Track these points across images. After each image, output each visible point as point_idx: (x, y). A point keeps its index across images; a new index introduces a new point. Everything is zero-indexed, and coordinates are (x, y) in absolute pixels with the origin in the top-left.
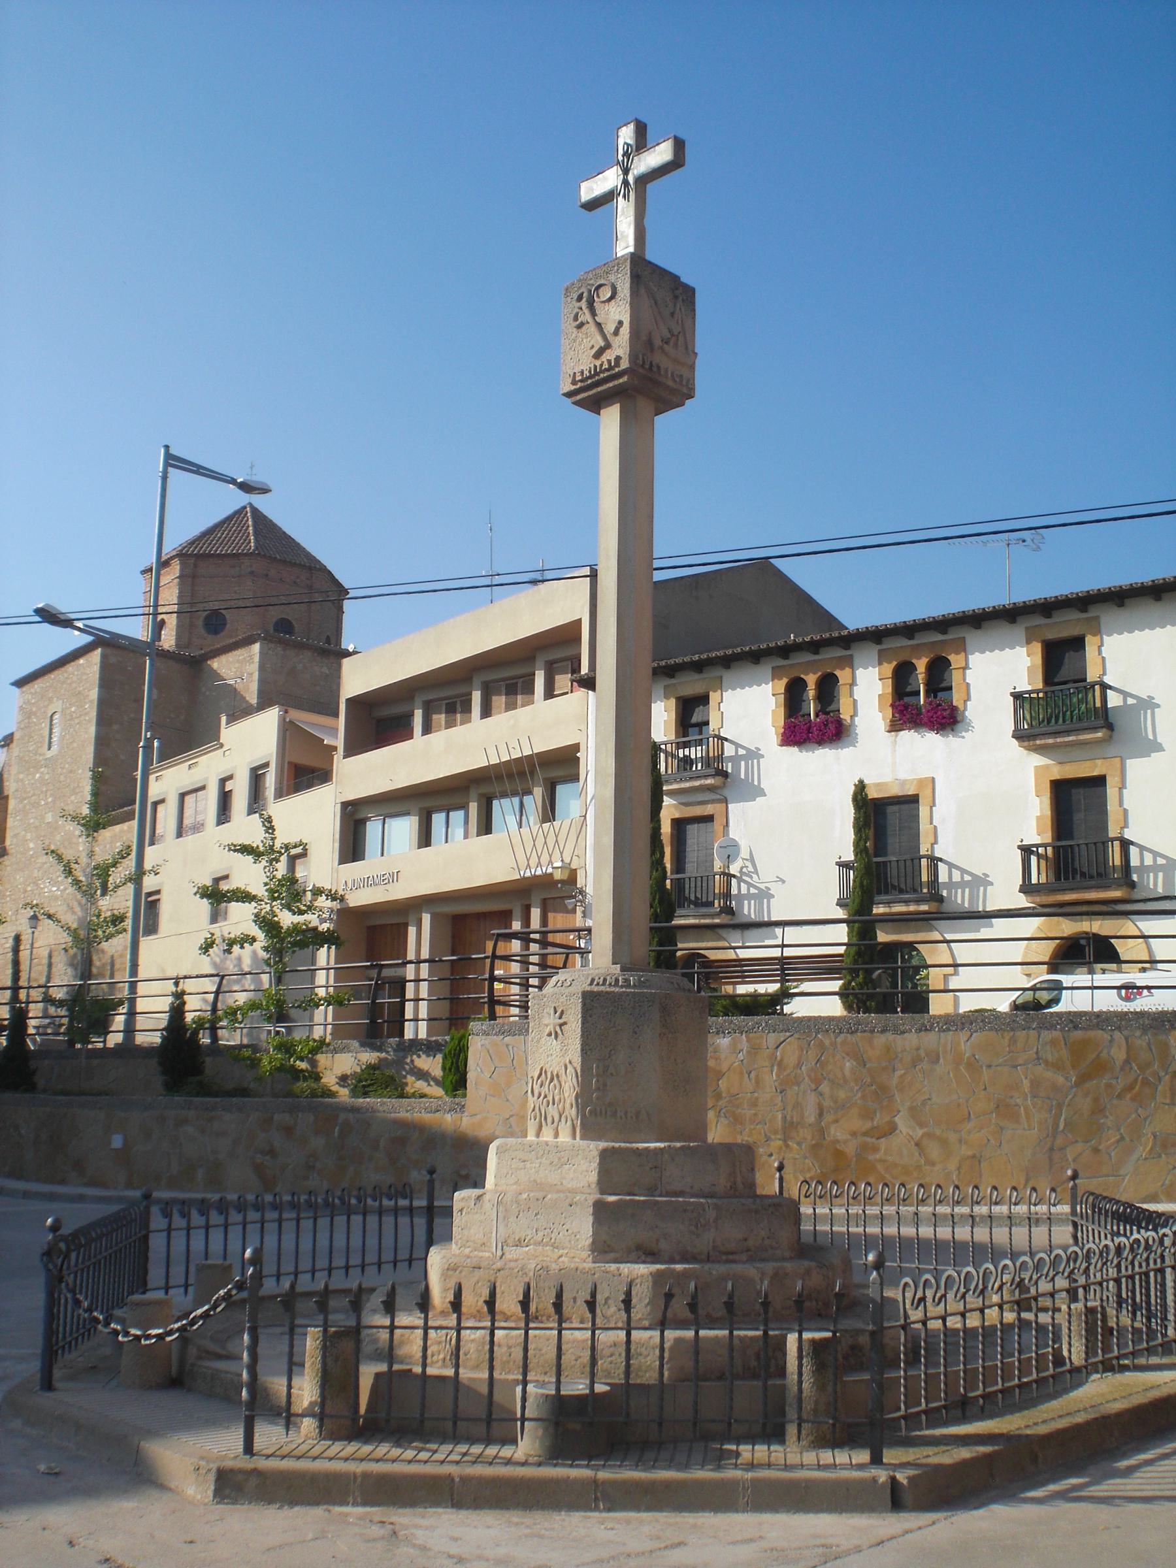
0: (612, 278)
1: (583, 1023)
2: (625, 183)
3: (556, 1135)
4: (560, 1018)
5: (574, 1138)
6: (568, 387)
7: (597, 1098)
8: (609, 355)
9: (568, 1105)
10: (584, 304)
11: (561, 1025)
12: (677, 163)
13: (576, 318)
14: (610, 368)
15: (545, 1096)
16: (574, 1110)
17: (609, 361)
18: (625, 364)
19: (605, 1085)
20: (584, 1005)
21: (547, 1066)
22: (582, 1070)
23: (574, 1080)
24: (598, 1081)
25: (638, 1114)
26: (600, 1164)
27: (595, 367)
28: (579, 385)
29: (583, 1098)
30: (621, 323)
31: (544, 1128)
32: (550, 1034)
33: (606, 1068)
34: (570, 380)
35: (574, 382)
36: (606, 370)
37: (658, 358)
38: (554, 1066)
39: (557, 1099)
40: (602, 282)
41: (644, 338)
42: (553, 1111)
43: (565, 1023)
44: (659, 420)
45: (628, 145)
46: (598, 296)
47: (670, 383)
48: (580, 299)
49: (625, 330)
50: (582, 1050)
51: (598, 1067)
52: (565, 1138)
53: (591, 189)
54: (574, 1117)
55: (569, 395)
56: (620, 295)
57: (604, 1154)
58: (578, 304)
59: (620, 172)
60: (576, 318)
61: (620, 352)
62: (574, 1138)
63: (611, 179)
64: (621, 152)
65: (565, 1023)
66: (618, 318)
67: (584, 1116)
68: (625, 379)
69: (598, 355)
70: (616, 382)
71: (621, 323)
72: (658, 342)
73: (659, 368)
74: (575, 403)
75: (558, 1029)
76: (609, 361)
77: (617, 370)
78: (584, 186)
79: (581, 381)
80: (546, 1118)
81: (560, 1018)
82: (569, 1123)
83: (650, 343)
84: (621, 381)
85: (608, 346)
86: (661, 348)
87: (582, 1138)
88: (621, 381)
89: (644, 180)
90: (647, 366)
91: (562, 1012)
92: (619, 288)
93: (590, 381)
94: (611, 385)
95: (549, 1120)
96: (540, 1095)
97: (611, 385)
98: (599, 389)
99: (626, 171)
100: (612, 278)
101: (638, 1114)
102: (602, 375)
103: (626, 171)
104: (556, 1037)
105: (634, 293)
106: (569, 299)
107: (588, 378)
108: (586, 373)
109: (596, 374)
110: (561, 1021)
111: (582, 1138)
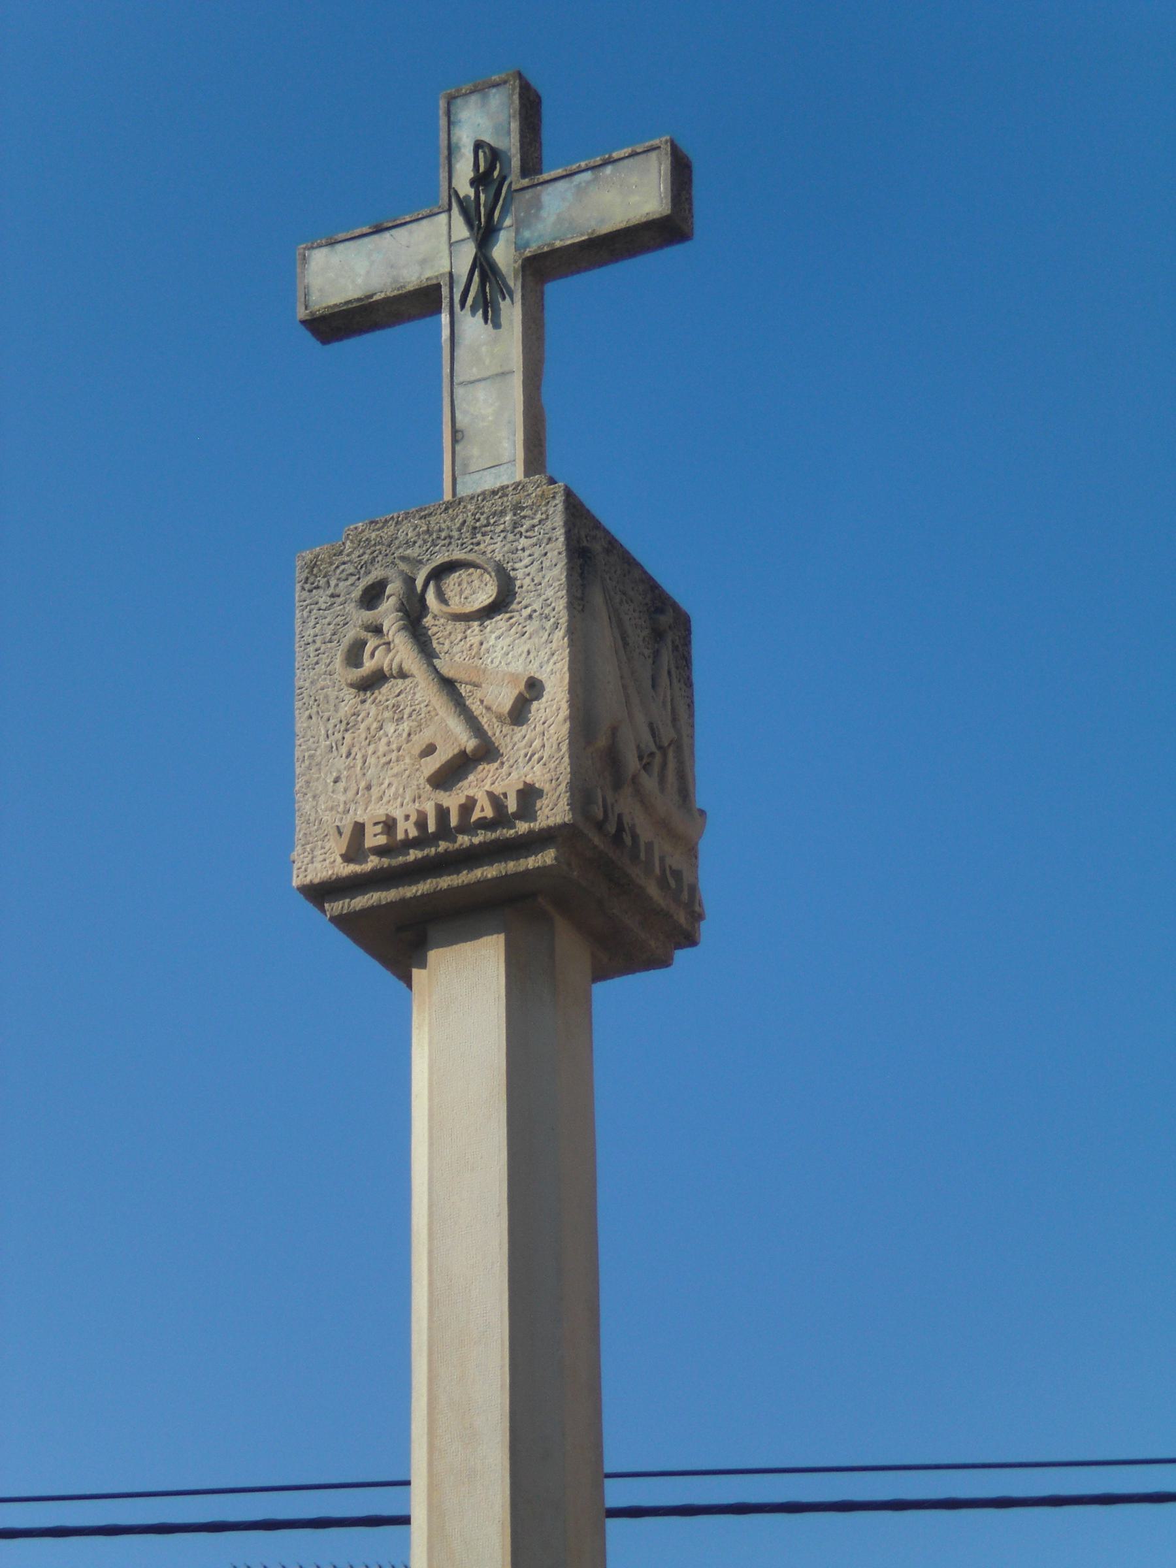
0: (495, 548)
2: (484, 266)
6: (323, 861)
8: (480, 786)
10: (388, 613)
12: (667, 231)
13: (354, 655)
14: (501, 818)
17: (497, 801)
18: (554, 811)
27: (442, 813)
28: (373, 862)
30: (534, 687)
34: (342, 845)
35: (354, 853)
36: (484, 824)
37: (627, 806)
40: (458, 555)
41: (602, 742)
44: (603, 992)
45: (495, 155)
46: (442, 598)
47: (653, 890)
48: (372, 596)
49: (553, 711)
53: (343, 272)
55: (320, 893)
56: (527, 600)
58: (367, 616)
59: (461, 230)
60: (354, 655)
61: (537, 775)
63: (430, 248)
64: (464, 170)
66: (521, 668)
68: (547, 857)
69: (446, 778)
70: (511, 866)
71: (534, 687)
72: (632, 763)
73: (635, 837)
74: (343, 922)
76: (497, 801)
77: (522, 827)
78: (319, 258)
79: (380, 851)
83: (612, 759)
84: (531, 862)
85: (487, 752)
86: (635, 779)
88: (531, 862)
89: (542, 267)
90: (612, 828)
92: (521, 575)
93: (414, 855)
94: (490, 872)
97: (490, 872)
98: (445, 882)
99: (485, 235)
100: (495, 548)
102: (463, 840)
103: (485, 235)
105: (578, 601)
106: (323, 598)
107: (409, 844)
108: (406, 829)
109: (445, 831)
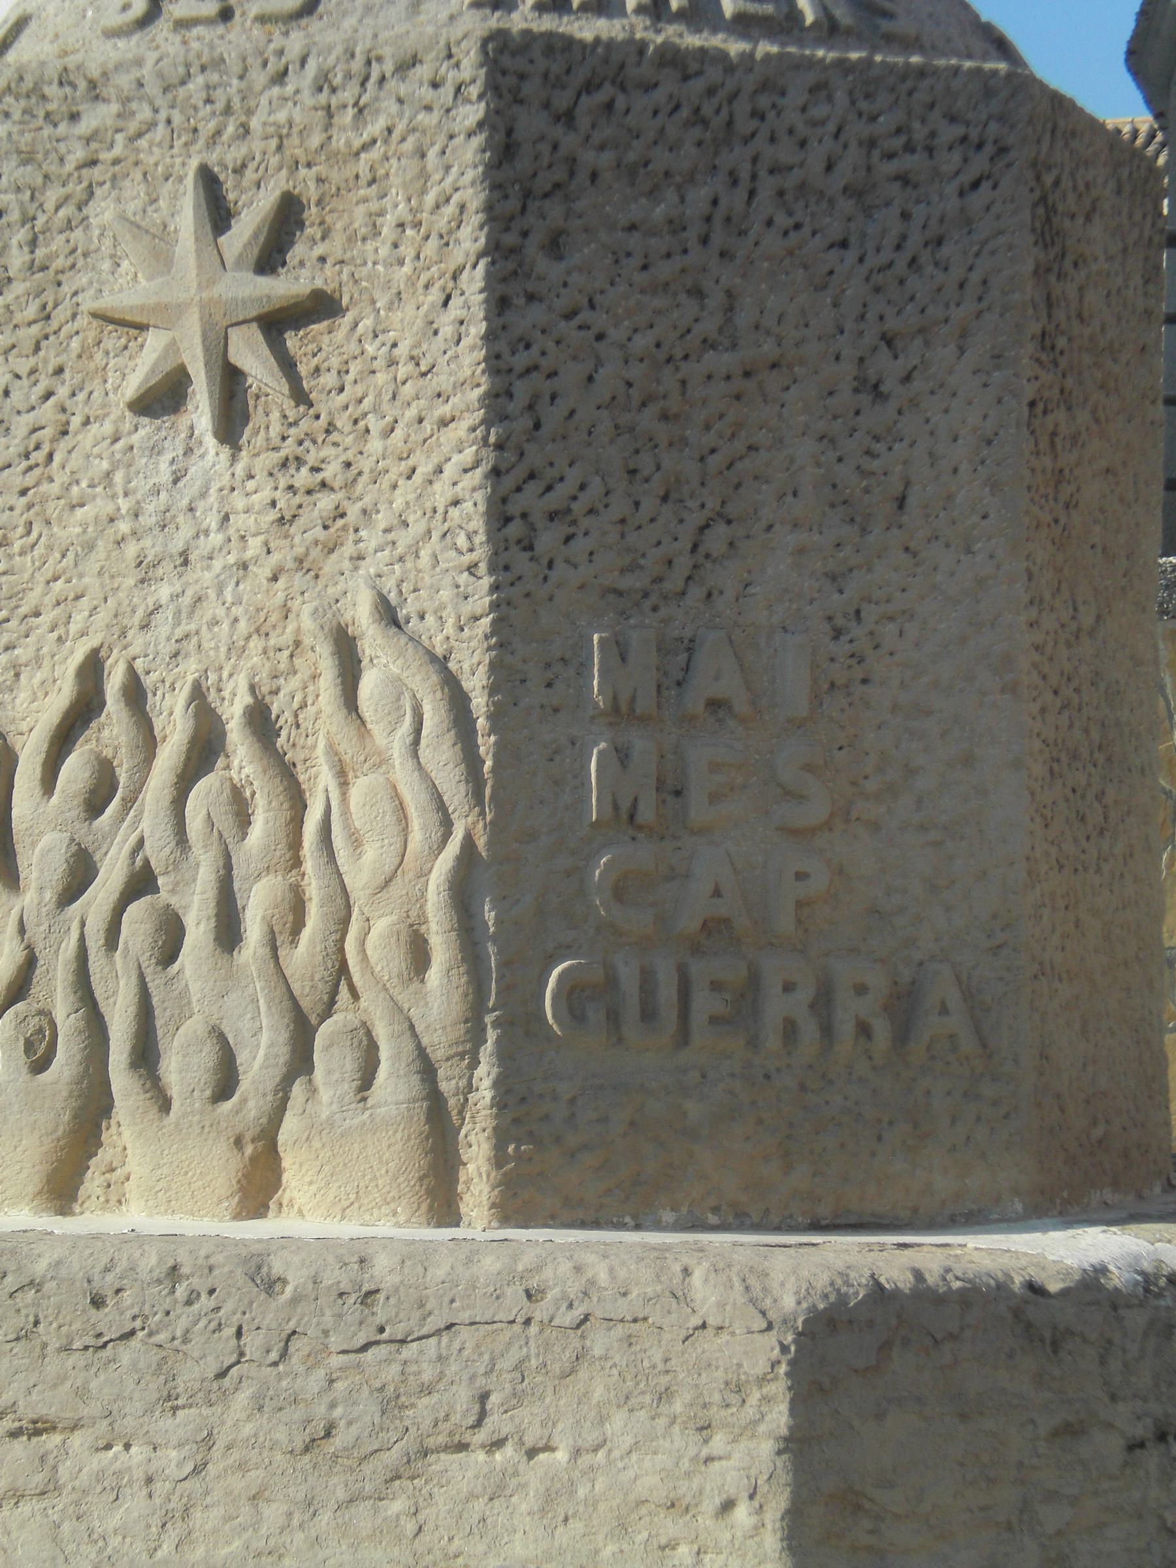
1: (499, 304)
3: (259, 1187)
4: (270, 257)
5: (443, 1206)
7: (621, 890)
9: (375, 944)
11: (276, 324)
15: (141, 883)
16: (440, 992)
19: (674, 791)
20: (504, 149)
21: (145, 649)
22: (504, 677)
23: (441, 756)
24: (621, 755)
25: (904, 1005)
26: (798, 1445)
29: (510, 900)
31: (128, 1130)
32: (163, 398)
33: (679, 659)
38: (210, 640)
39: (258, 906)
42: (221, 1000)
43: (322, 307)
50: (499, 515)
51: (618, 650)
52: (341, 1203)
54: (439, 1038)
57: (843, 1360)
62: (443, 1206)
65: (322, 307)
67: (521, 1026)
75: (251, 356)
80: (146, 1055)
81: (270, 257)
82: (393, 1084)
87: (515, 1207)
91: (287, 219)
95: (183, 1065)
96: (80, 874)
101: (904, 1005)
104: (232, 421)
110: (286, 287)
111: (515, 1207)
